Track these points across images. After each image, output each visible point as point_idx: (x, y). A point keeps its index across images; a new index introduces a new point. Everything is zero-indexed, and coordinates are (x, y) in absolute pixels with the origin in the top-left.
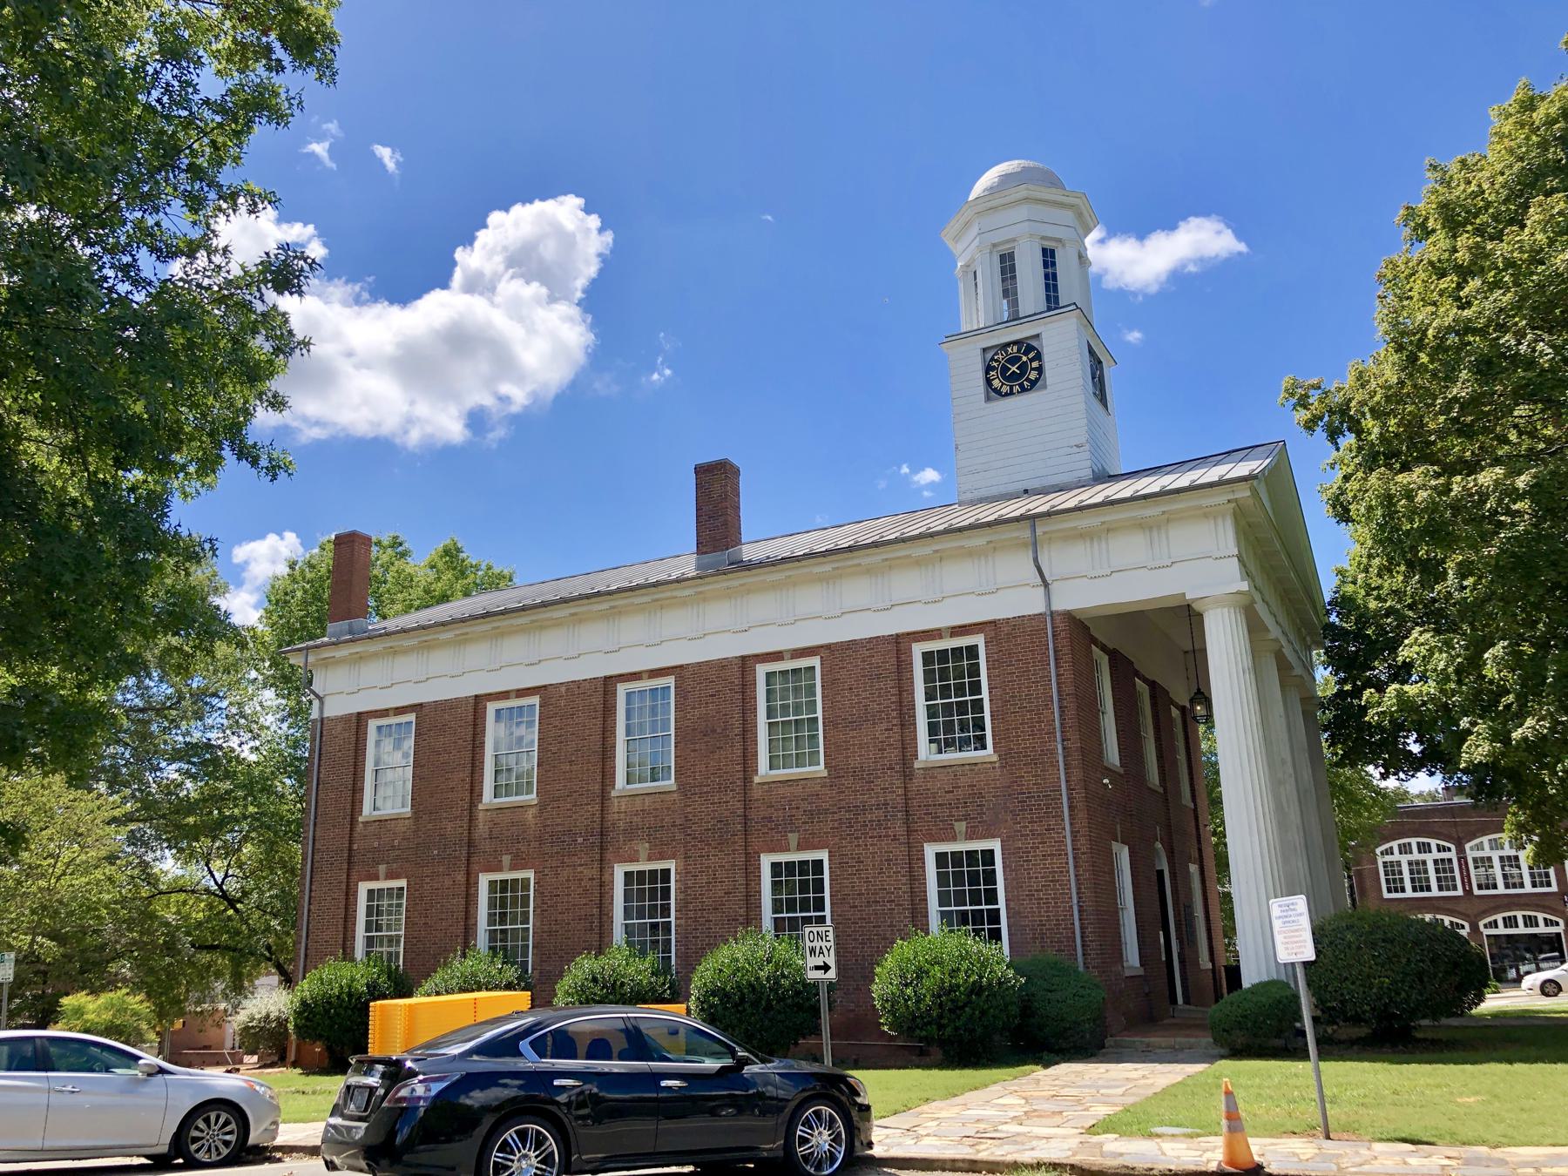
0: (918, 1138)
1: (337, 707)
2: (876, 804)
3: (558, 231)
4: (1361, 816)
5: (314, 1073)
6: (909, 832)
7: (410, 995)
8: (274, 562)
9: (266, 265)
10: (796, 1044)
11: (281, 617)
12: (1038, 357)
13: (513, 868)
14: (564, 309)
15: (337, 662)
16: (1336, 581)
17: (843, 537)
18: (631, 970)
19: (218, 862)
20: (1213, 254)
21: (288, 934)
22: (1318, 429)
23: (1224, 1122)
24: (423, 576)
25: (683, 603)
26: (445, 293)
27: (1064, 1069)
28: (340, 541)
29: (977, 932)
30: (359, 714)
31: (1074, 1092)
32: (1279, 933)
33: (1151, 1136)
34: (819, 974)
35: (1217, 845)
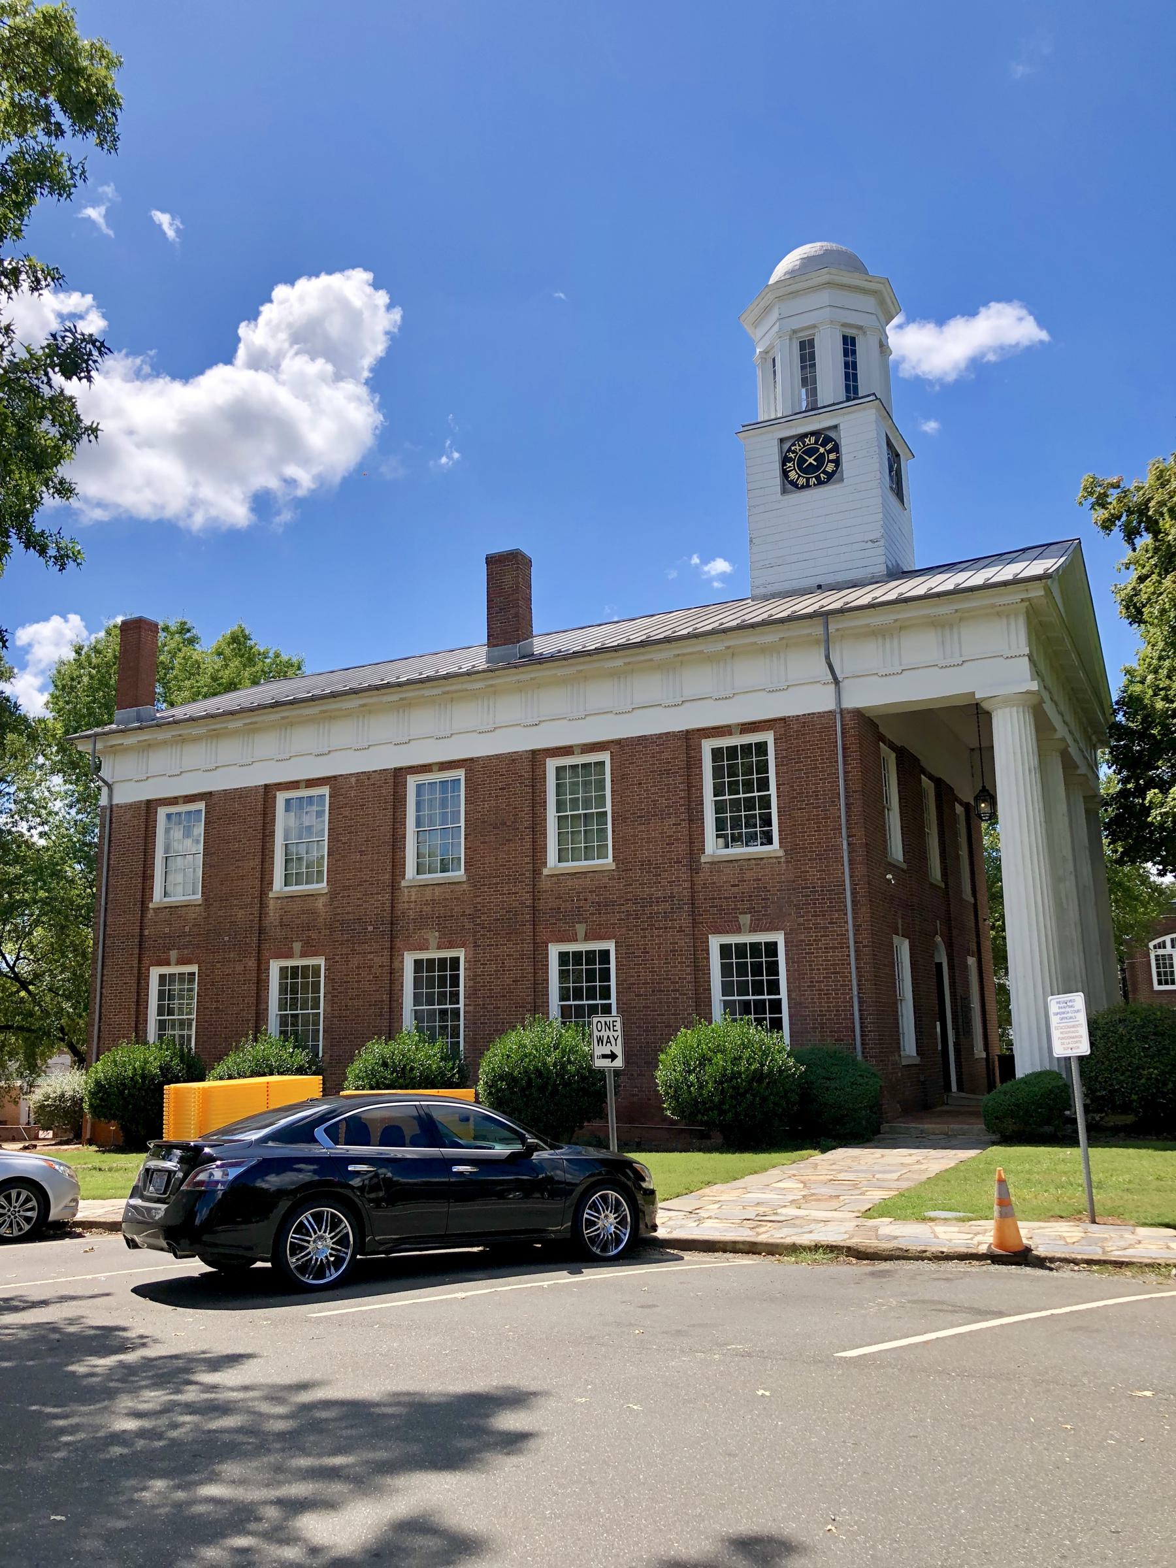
0: (700, 1221)
1: (126, 795)
2: (663, 899)
3: (344, 303)
4: (1136, 911)
5: (109, 1151)
6: (695, 924)
7: (202, 1079)
8: (57, 645)
9: (53, 349)
10: (581, 1127)
11: (67, 703)
12: (836, 449)
13: (303, 955)
14: (350, 387)
15: (126, 749)
16: (1124, 680)
17: (636, 632)
18: (421, 1055)
19: (10, 945)
20: (1013, 342)
21: (80, 1016)
22: (1116, 529)
23: (996, 1207)
24: (212, 664)
25: (474, 696)
26: (229, 368)
27: (842, 1155)
28: (126, 627)
29: (759, 1021)
30: (149, 801)
31: (851, 1176)
32: (1057, 1028)
33: (925, 1219)
34: (606, 1063)
35: (995, 938)
